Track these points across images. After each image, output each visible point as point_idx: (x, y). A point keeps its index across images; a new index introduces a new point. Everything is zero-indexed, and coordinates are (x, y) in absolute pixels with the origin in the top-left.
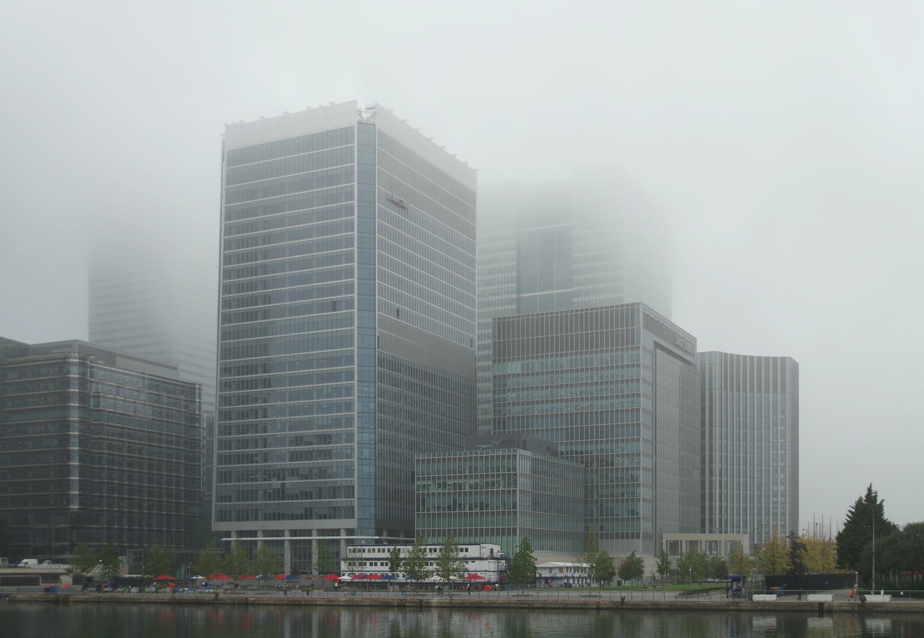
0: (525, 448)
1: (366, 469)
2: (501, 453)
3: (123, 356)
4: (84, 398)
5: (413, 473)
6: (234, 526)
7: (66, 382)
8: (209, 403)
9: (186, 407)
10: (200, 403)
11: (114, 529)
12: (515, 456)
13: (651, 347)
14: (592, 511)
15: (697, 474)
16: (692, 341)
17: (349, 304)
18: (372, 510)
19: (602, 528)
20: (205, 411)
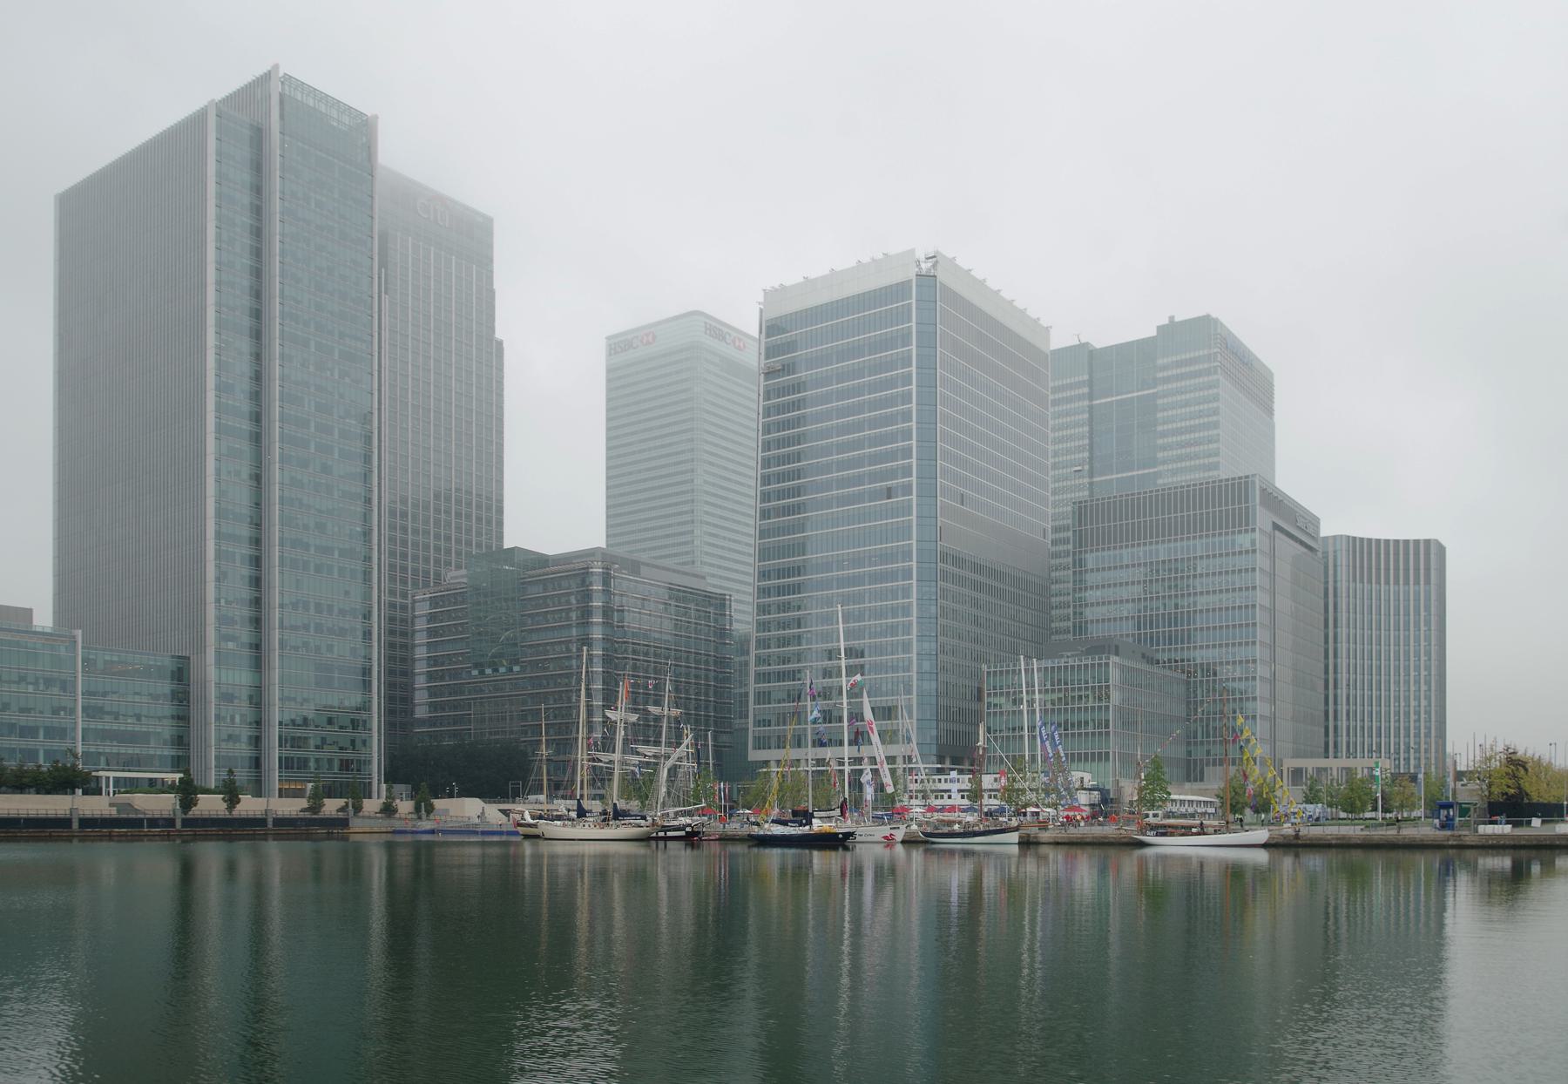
0: (1117, 654)
1: (926, 685)
2: (1090, 662)
3: (648, 565)
4: (607, 612)
5: (980, 690)
6: (772, 754)
7: (587, 595)
8: (743, 619)
9: (716, 621)
12: (1107, 665)
13: (1269, 528)
14: (1196, 732)
15: (1321, 689)
16: (1315, 522)
17: (907, 489)
18: (934, 733)
19: (1208, 753)
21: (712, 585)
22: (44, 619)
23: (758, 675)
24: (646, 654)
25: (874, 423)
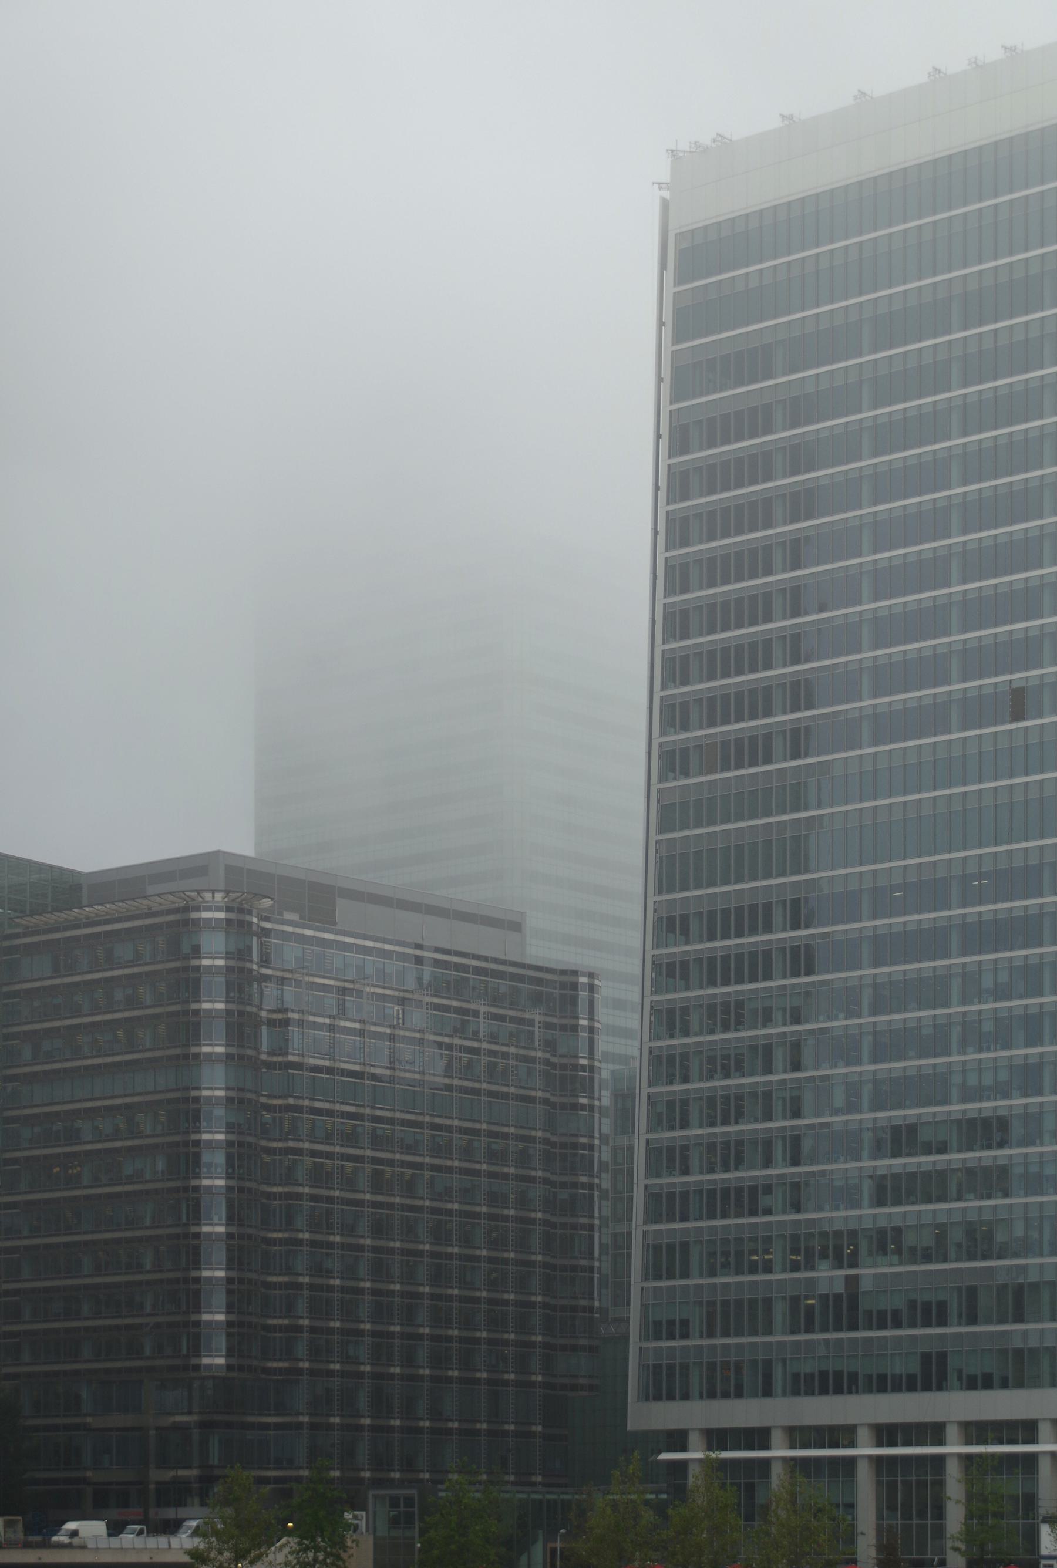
4: (240, 1028)
8: (620, 1032)
9: (550, 1045)
10: (591, 1030)
11: (330, 1427)
20: (607, 1057)
21: (542, 949)
22: (620, 1032)
23: (653, 1198)
24: (351, 1138)
25: (981, 561)
